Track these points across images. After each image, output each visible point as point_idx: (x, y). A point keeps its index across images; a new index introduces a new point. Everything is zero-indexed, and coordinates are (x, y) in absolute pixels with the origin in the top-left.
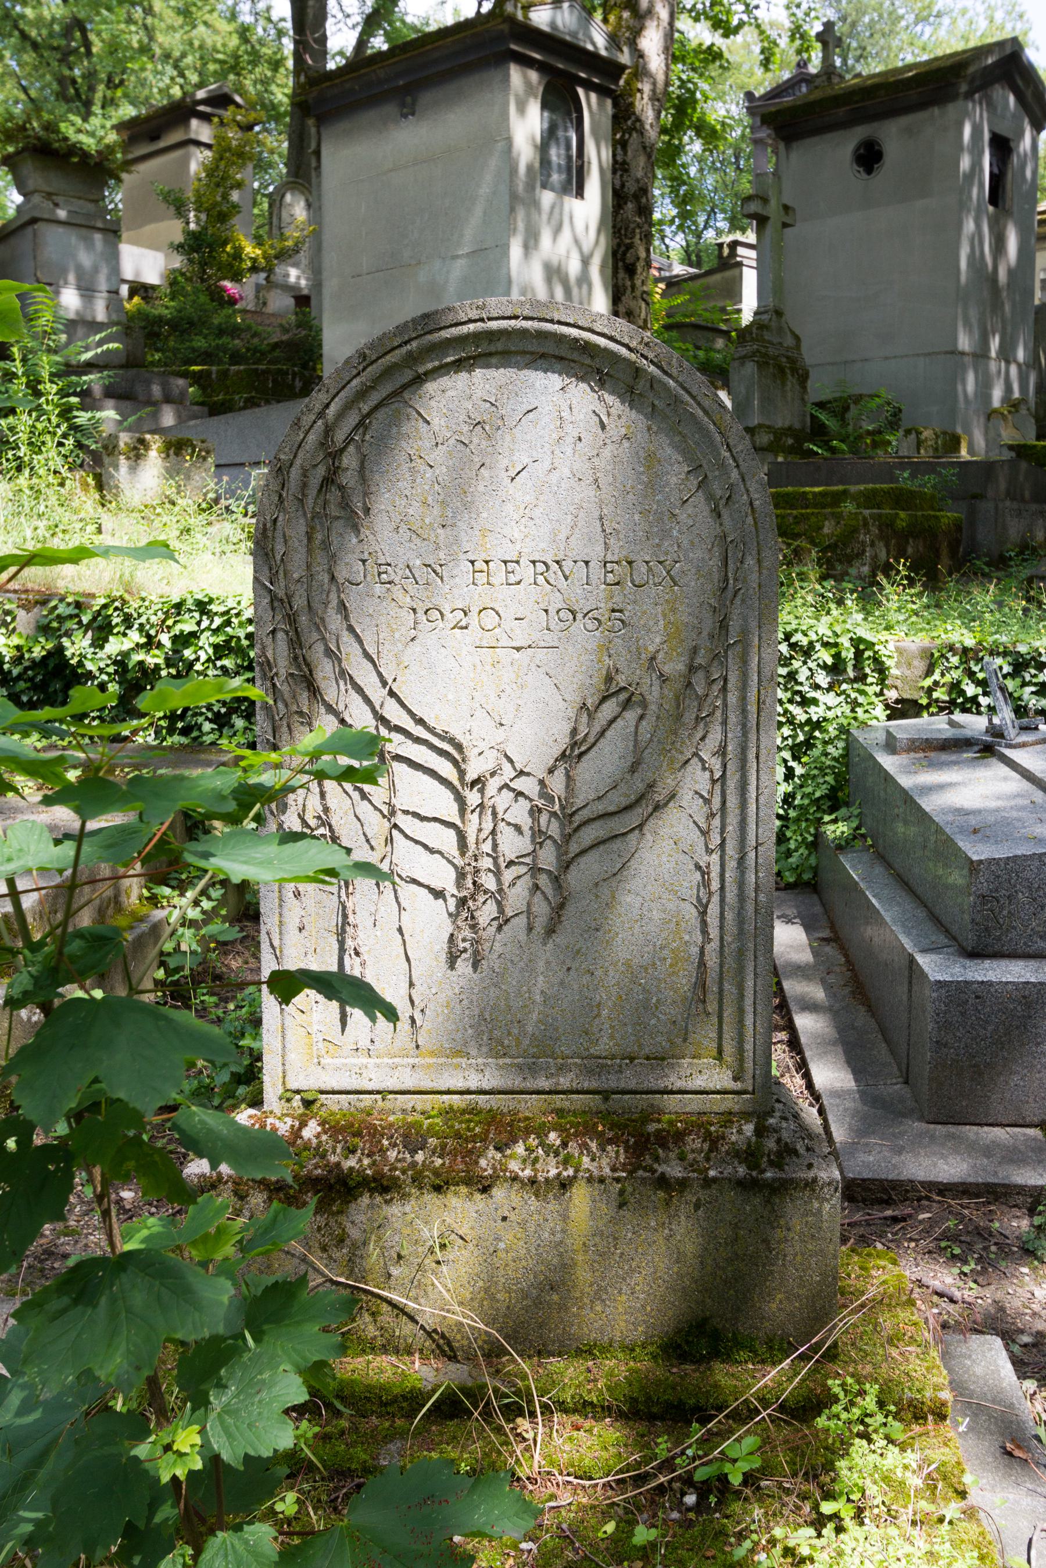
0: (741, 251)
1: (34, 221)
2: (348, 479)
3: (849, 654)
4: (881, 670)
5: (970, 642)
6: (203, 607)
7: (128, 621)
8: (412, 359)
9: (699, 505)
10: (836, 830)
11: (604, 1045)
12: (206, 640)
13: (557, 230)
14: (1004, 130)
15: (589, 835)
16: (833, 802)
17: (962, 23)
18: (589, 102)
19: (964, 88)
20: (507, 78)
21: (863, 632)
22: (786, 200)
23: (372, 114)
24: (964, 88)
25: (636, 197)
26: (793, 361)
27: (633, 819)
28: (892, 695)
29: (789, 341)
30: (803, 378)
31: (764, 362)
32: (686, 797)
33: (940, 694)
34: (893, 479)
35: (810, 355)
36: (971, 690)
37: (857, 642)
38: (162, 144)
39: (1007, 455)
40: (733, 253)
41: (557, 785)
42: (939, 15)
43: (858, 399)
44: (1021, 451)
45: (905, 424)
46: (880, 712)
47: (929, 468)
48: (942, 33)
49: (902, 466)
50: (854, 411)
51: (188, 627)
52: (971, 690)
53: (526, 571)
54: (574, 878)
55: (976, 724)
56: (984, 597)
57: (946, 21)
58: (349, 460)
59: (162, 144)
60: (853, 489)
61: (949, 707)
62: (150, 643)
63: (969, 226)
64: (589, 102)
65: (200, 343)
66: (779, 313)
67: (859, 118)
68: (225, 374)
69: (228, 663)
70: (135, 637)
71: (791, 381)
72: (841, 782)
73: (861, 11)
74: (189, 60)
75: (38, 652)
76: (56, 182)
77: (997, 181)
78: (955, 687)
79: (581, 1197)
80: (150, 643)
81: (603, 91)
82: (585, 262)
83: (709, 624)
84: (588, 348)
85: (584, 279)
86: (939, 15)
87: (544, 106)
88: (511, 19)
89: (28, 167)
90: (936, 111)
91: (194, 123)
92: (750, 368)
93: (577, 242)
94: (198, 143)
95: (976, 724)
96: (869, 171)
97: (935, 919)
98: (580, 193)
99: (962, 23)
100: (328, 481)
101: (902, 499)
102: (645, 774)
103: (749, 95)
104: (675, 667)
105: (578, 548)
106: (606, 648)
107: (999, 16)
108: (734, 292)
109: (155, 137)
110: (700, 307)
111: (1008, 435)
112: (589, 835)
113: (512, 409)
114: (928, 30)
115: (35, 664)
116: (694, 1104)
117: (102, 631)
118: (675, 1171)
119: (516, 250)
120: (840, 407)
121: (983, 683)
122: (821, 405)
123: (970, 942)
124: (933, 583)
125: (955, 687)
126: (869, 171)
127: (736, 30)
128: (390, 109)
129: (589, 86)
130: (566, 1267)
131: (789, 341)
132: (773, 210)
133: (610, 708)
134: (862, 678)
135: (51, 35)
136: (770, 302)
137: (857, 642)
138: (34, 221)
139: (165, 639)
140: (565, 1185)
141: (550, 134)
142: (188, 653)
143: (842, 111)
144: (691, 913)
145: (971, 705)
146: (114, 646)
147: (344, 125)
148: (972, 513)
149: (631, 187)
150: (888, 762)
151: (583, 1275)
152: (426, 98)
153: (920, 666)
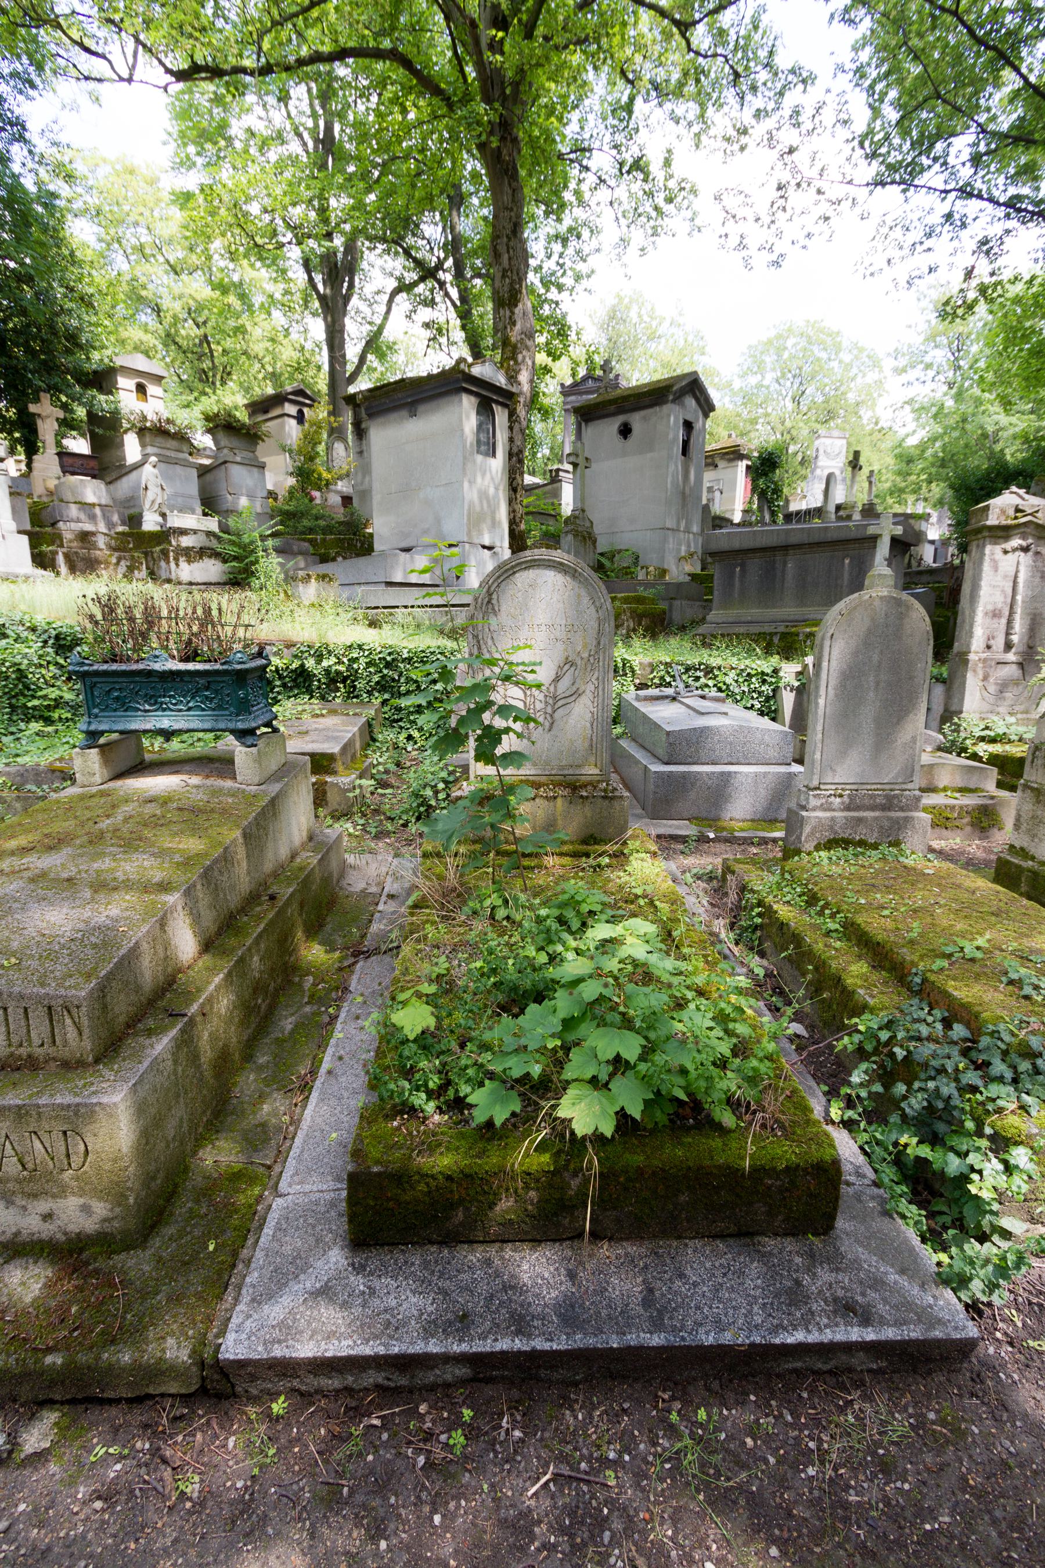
0: (561, 474)
1: (225, 462)
2: (494, 602)
3: (620, 665)
4: (633, 671)
5: (668, 660)
6: (360, 647)
7: (330, 652)
8: (513, 567)
9: (593, 609)
10: (618, 730)
11: (564, 763)
12: (363, 661)
13: (484, 475)
14: (689, 418)
15: (560, 703)
16: (615, 721)
17: (671, 341)
18: (498, 410)
19: (671, 397)
20: (461, 401)
21: (626, 656)
22: (587, 454)
23: (394, 416)
24: (671, 397)
25: (517, 454)
26: (589, 534)
27: (572, 698)
28: (637, 681)
29: (588, 524)
30: (594, 542)
31: (576, 534)
32: (588, 692)
33: (656, 681)
34: (636, 591)
35: (597, 529)
36: (668, 679)
37: (623, 660)
38: (270, 415)
39: (688, 579)
40: (557, 475)
41: (552, 689)
42: (659, 337)
43: (620, 551)
44: (693, 576)
45: (641, 563)
46: (632, 688)
47: (653, 586)
48: (661, 347)
49: (640, 584)
50: (617, 558)
51: (355, 655)
52: (668, 679)
53: (543, 628)
54: (557, 715)
55: (670, 691)
56: (674, 641)
57: (663, 340)
58: (494, 596)
59: (270, 415)
60: (619, 595)
61: (661, 685)
62: (340, 662)
63: (672, 468)
64: (498, 410)
65: (306, 523)
66: (583, 511)
67: (621, 411)
68: (324, 540)
69: (372, 670)
70: (333, 660)
71: (589, 543)
72: (618, 715)
73: (619, 336)
74: (267, 359)
75: (294, 666)
76: (235, 442)
77: (686, 444)
78: (662, 678)
79: (559, 801)
80: (340, 662)
81: (504, 405)
82: (497, 489)
83: (595, 643)
84: (561, 564)
85: (496, 495)
86: (659, 337)
87: (478, 413)
88: (463, 372)
89: (221, 435)
90: (657, 408)
91: (287, 405)
92: (570, 537)
93: (492, 479)
94: (289, 416)
95: (670, 691)
96: (625, 438)
97: (655, 756)
98: (494, 455)
99: (671, 341)
100: (489, 602)
101: (640, 600)
102: (576, 686)
103: (562, 385)
104: (585, 655)
105: (558, 621)
106: (566, 650)
107: (690, 338)
108: (557, 494)
109: (266, 412)
110: (541, 503)
111: (688, 568)
112: (560, 703)
113: (540, 581)
114: (654, 345)
115: (292, 671)
116: (589, 778)
117: (319, 658)
118: (585, 794)
119: (466, 485)
120: (611, 556)
121: (673, 677)
122: (602, 554)
123: (666, 759)
124: (654, 636)
125: (662, 678)
126: (625, 438)
127: (559, 357)
128: (404, 413)
129: (498, 403)
130: (555, 820)
131: (588, 524)
132: (581, 461)
133: (567, 667)
134: (625, 675)
135: (195, 345)
136: (579, 505)
137: (623, 660)
138: (225, 462)
139: (345, 660)
140: (555, 798)
141: (480, 427)
142: (355, 666)
143: (612, 408)
144: (588, 725)
145: (669, 685)
146: (325, 663)
147: (381, 420)
148: (671, 606)
149: (515, 450)
150: (636, 704)
151: (560, 822)
152: (421, 408)
153: (648, 670)
